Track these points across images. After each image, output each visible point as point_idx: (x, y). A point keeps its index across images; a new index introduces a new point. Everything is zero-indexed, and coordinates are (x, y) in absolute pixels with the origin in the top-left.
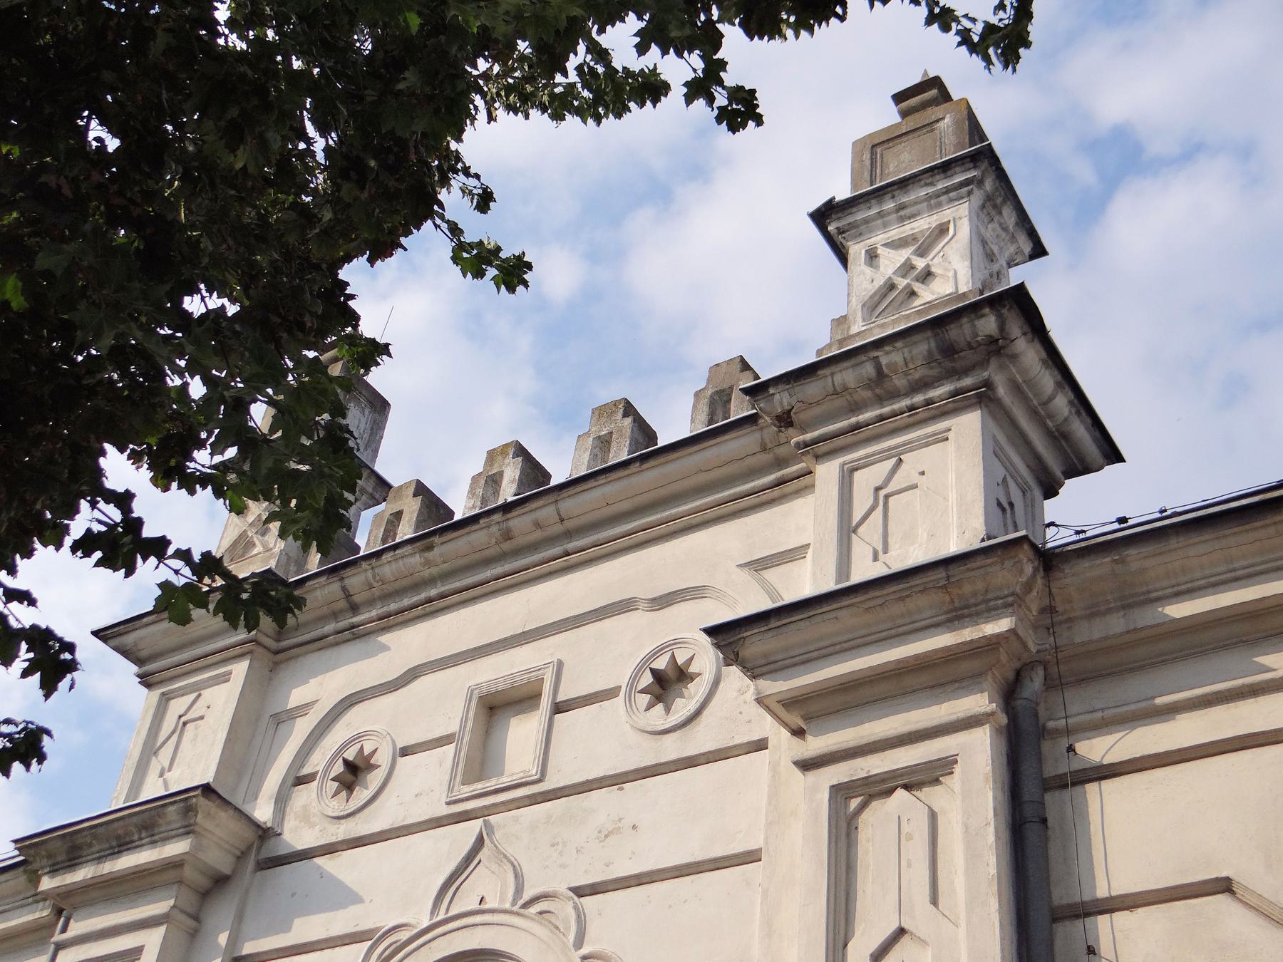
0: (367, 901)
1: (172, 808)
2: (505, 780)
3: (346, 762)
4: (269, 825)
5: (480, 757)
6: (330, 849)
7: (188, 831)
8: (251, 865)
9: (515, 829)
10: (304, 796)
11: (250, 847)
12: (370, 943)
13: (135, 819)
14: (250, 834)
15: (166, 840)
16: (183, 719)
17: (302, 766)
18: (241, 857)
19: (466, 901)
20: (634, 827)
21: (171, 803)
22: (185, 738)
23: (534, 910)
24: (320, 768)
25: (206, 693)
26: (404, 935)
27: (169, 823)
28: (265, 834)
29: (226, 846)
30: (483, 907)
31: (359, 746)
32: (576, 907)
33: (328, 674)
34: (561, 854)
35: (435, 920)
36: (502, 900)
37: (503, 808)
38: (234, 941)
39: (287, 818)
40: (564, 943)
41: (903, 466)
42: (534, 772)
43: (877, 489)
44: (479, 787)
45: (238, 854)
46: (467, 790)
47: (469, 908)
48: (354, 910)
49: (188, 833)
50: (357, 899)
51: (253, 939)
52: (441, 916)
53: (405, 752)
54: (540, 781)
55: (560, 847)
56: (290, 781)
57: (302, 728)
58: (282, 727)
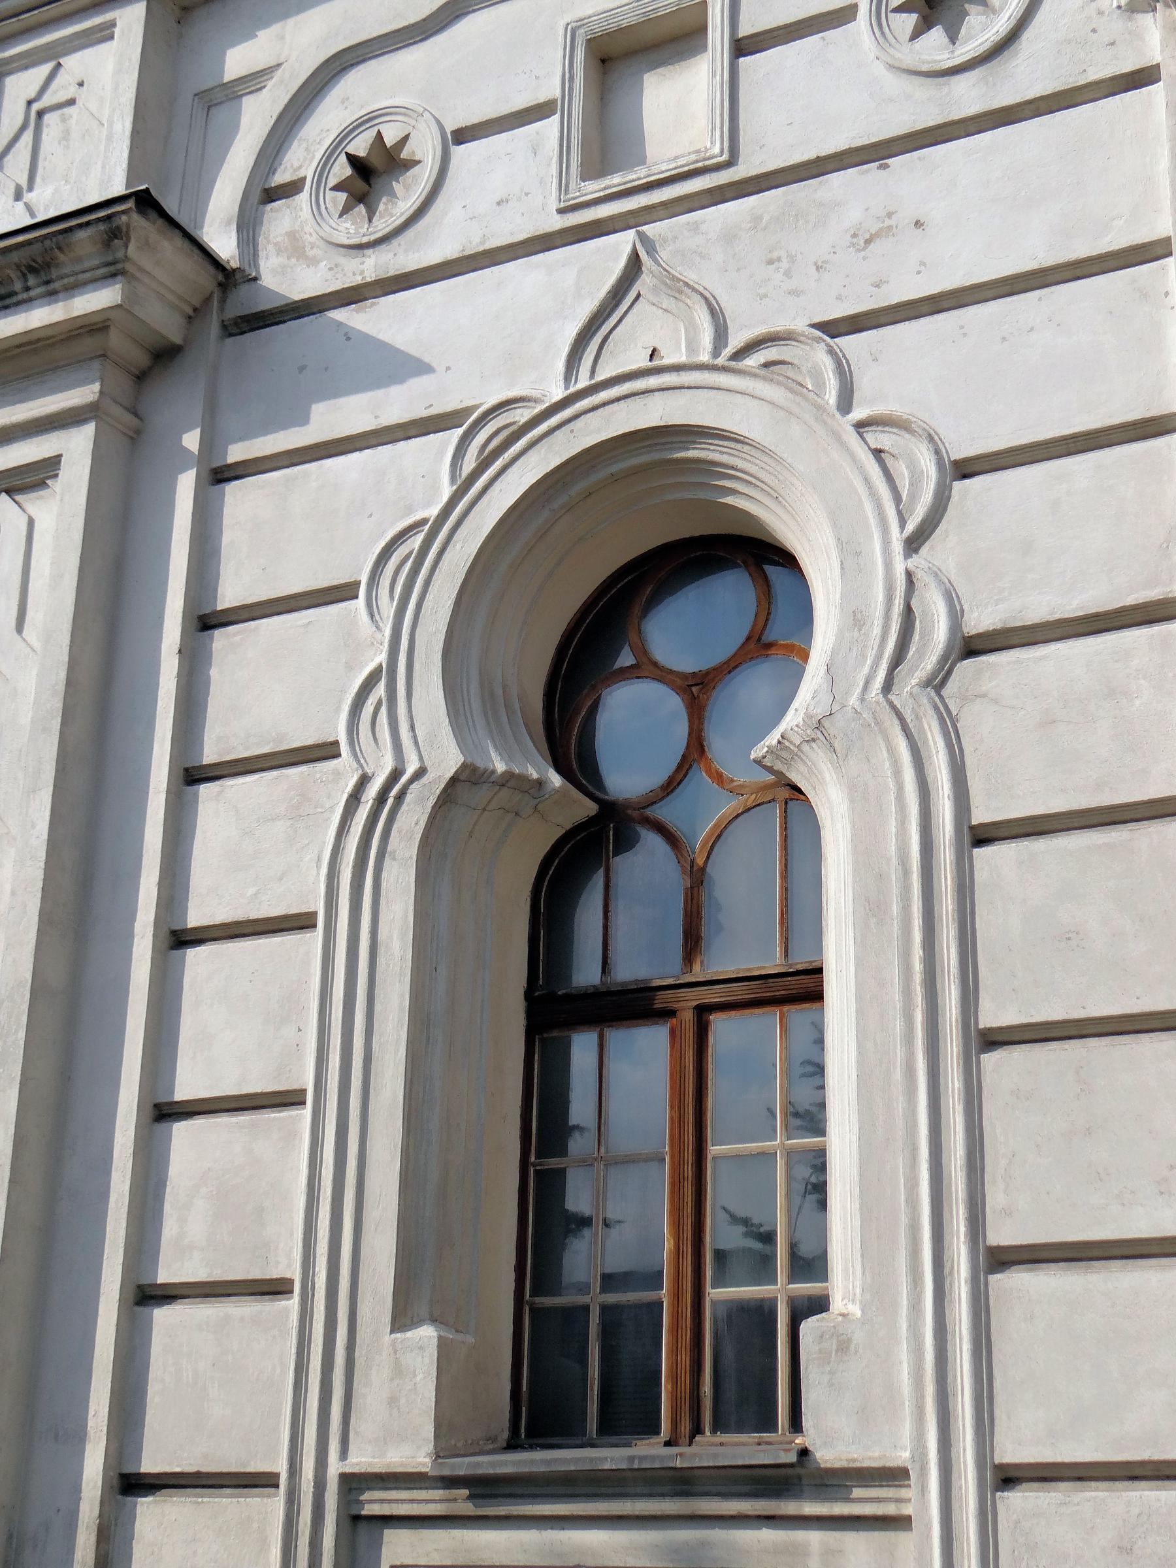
0: (440, 369)
1: (82, 234)
2: (639, 175)
3: (353, 160)
4: (235, 264)
5: (605, 138)
6: (352, 296)
7: (113, 271)
8: (215, 329)
9: (696, 243)
10: (281, 220)
11: (208, 300)
12: (460, 431)
13: (15, 257)
14: (206, 279)
15: (74, 288)
16: (36, 107)
17: (272, 171)
18: (195, 316)
19: (626, 352)
20: (918, 224)
21: (80, 226)
22: (45, 137)
23: (753, 361)
24: (309, 172)
25: (73, 63)
26: (522, 415)
27: (79, 260)
28: (228, 278)
29: (171, 298)
30: (656, 363)
31: (372, 133)
32: (831, 352)
33: (291, 22)
34: (788, 274)
35: (572, 390)
36: (692, 347)
37: (662, 213)
38: (207, 443)
39: (262, 254)
40: (818, 407)
41: (62, 71)
42: (716, 150)
43: (30, 103)
44: (615, 181)
45: (190, 311)
46: (593, 188)
47: (634, 366)
48: (417, 385)
49: (113, 275)
50: (422, 368)
51: (241, 439)
52: (583, 382)
53: (462, 136)
54: (729, 164)
55: (784, 264)
56: (257, 194)
57: (256, 116)
58: (221, 115)
